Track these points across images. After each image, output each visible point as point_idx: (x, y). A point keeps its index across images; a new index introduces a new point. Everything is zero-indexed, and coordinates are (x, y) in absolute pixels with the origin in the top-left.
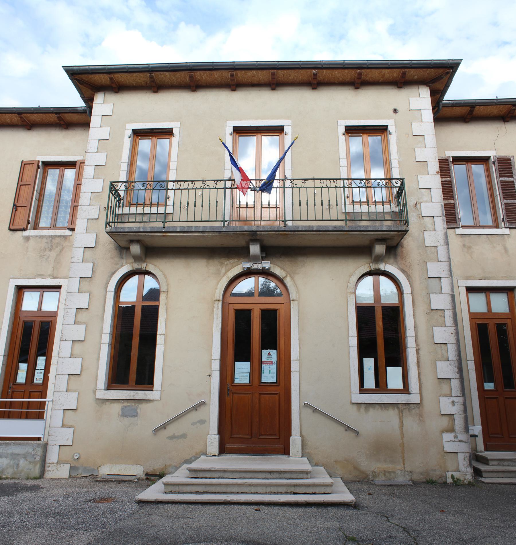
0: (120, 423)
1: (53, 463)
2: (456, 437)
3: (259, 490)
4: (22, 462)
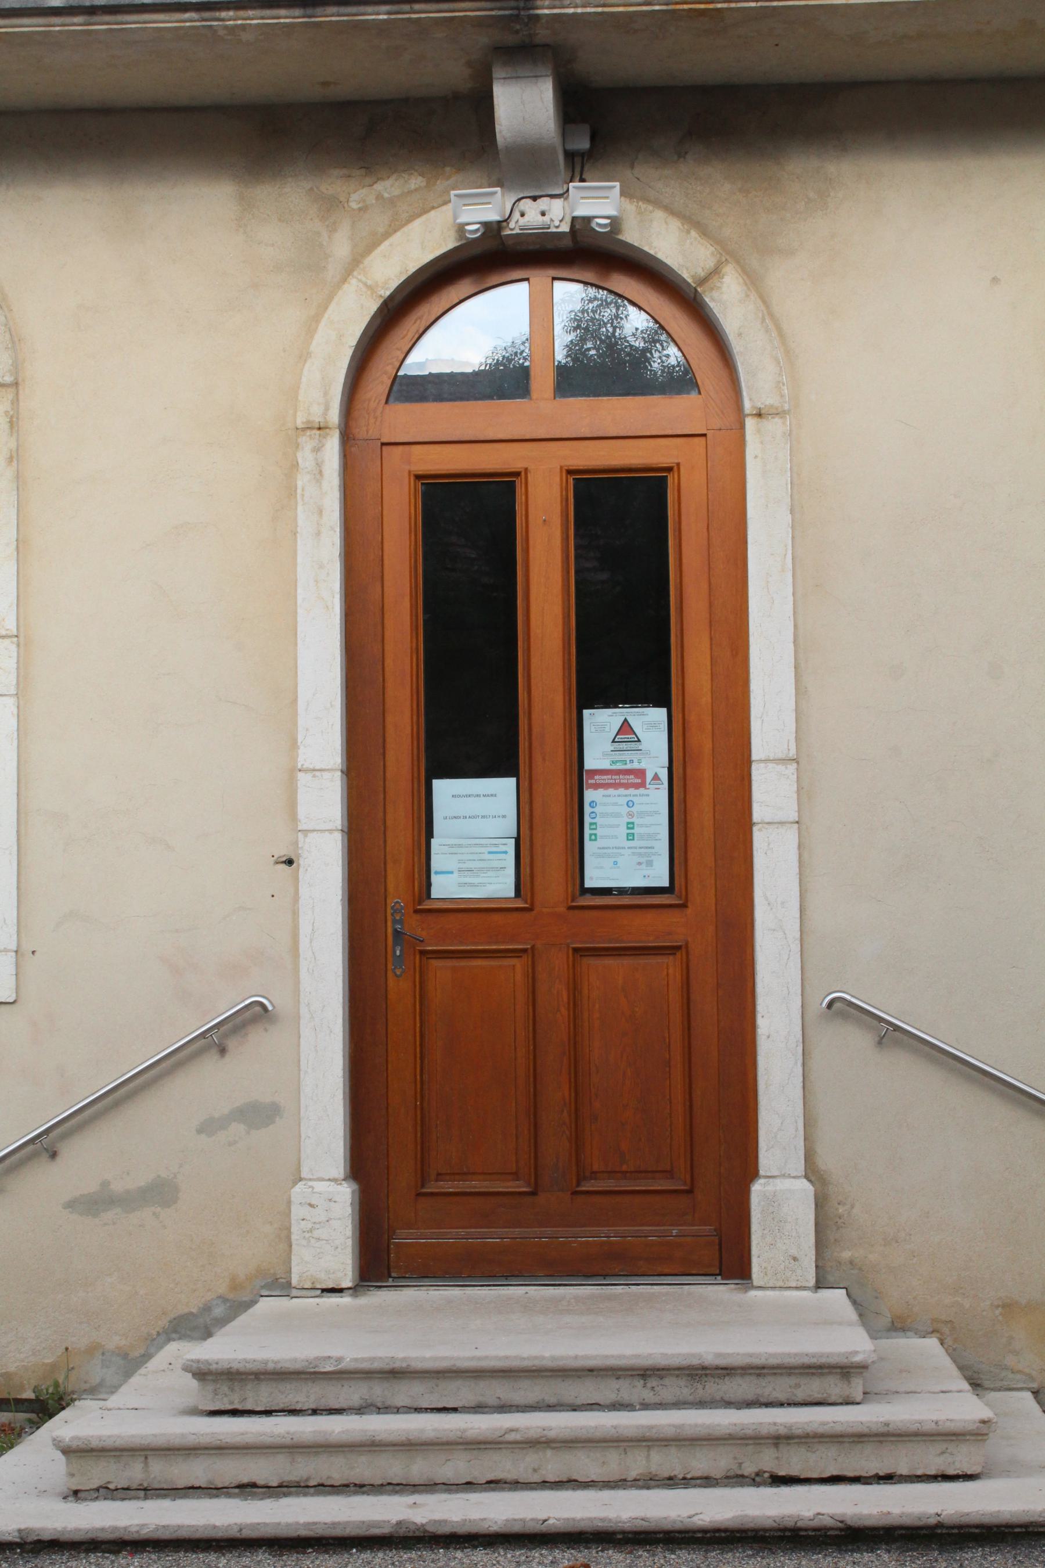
3: (586, 1464)
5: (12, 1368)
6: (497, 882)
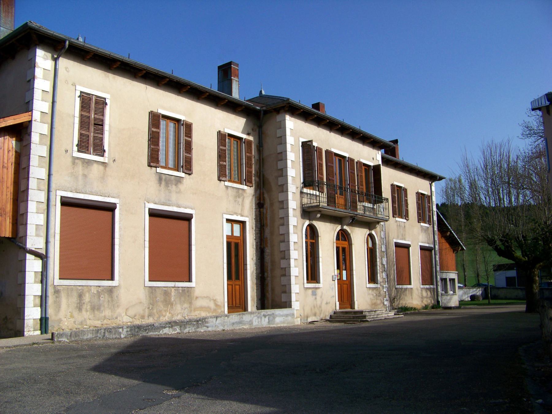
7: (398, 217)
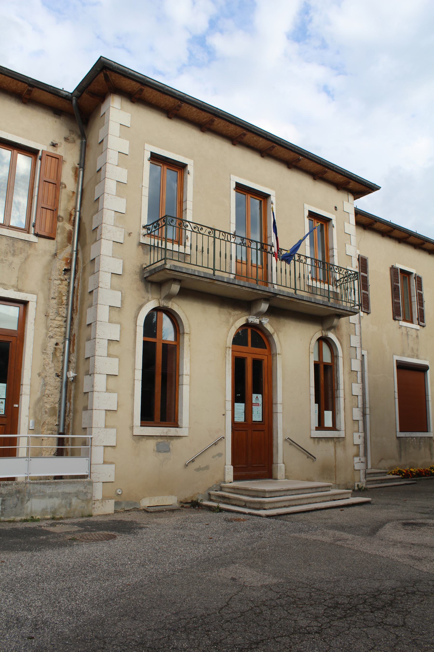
0: (156, 458)
1: (98, 500)
2: (360, 459)
3: (317, 500)
4: (74, 501)
5: (186, 497)
6: (260, 419)
7: (404, 320)
